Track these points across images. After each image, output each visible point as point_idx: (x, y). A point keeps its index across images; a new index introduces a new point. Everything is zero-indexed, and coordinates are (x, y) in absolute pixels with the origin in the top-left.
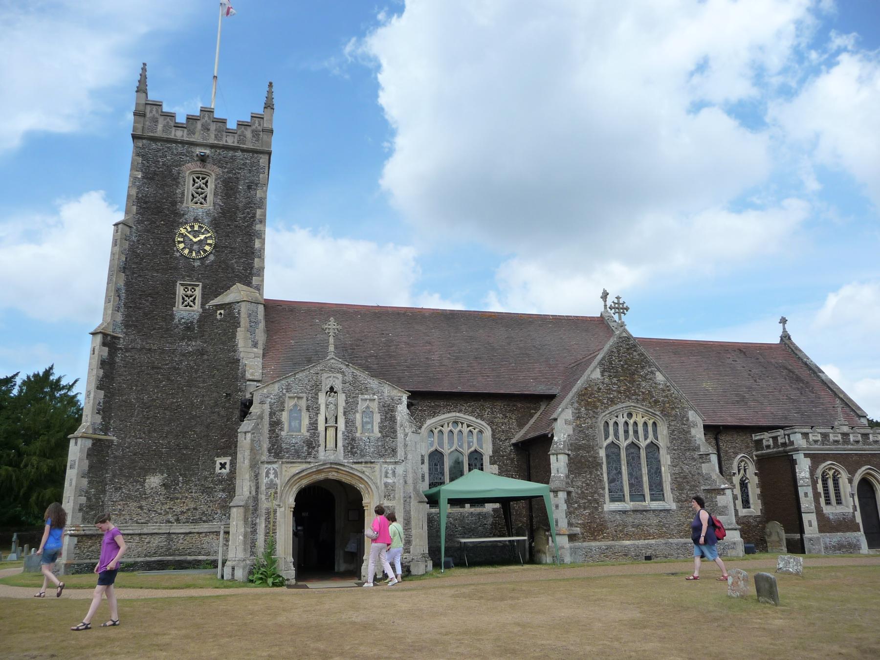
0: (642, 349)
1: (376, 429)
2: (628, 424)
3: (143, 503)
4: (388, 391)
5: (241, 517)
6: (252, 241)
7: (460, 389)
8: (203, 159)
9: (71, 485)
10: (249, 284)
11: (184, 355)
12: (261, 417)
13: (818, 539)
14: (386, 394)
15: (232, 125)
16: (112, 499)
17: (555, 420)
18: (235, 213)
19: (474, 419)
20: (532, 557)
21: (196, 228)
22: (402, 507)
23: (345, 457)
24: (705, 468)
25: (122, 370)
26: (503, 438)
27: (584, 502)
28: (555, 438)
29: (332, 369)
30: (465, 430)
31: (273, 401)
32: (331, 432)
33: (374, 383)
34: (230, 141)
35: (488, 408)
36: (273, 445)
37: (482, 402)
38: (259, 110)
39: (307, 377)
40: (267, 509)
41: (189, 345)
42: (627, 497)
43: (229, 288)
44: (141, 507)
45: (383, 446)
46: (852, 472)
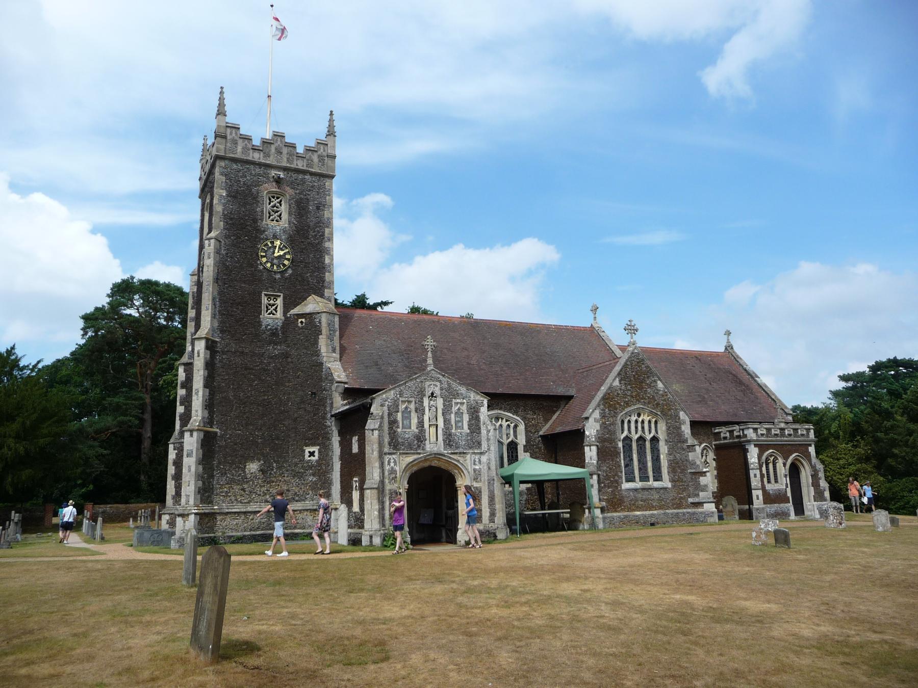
0: (648, 362)
1: (466, 426)
2: (639, 423)
3: (245, 486)
4: (473, 396)
6: (322, 257)
7: (526, 392)
8: (278, 181)
9: (189, 470)
10: (322, 296)
11: (272, 358)
13: (763, 508)
14: (472, 398)
15: (300, 150)
16: (219, 481)
17: (587, 418)
18: (308, 231)
20: (571, 525)
24: (691, 456)
25: (221, 370)
26: (533, 431)
27: (609, 482)
28: (587, 433)
29: (433, 379)
30: (505, 424)
32: (433, 429)
33: (463, 390)
34: (300, 165)
36: (392, 440)
37: (517, 401)
38: (322, 137)
42: (637, 479)
43: (306, 299)
44: (243, 490)
46: (786, 458)
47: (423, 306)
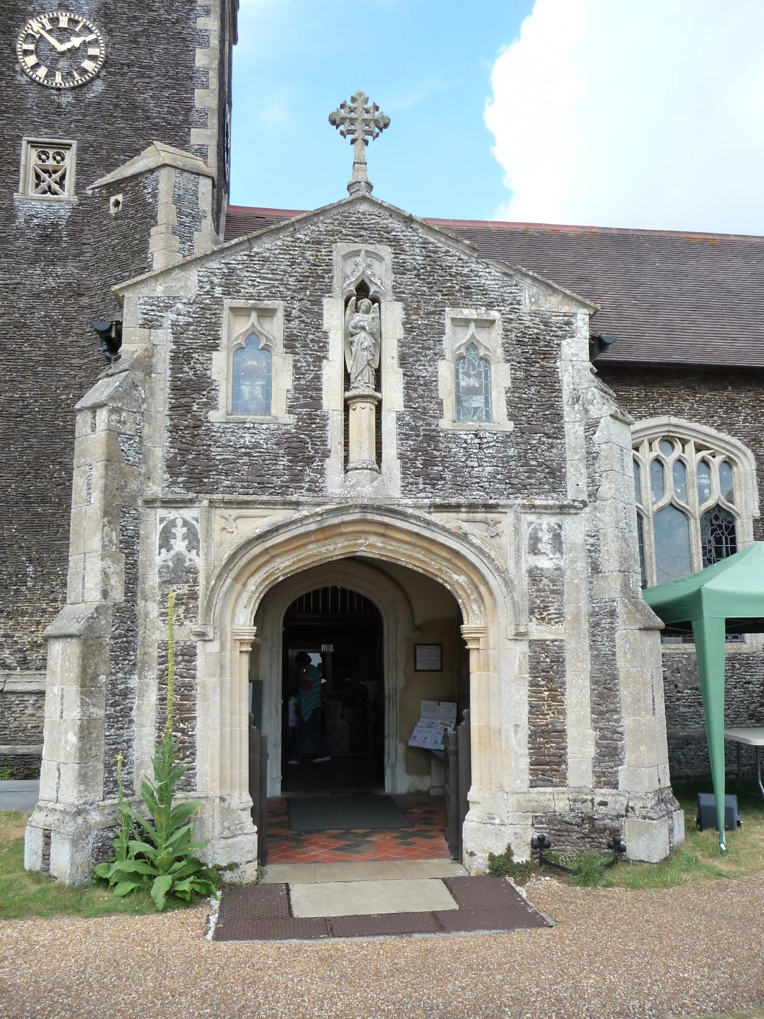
5: (74, 673)
11: (38, 296)
12: (145, 365)
14: (526, 307)
19: (713, 431)
21: (63, 23)
22: (586, 642)
23: (406, 489)
30: (693, 458)
31: (182, 320)
32: (362, 415)
35: (746, 405)
36: (184, 452)
39: (286, 250)
40: (164, 646)
41: (47, 275)
45: (522, 458)
47: (732, 557)
